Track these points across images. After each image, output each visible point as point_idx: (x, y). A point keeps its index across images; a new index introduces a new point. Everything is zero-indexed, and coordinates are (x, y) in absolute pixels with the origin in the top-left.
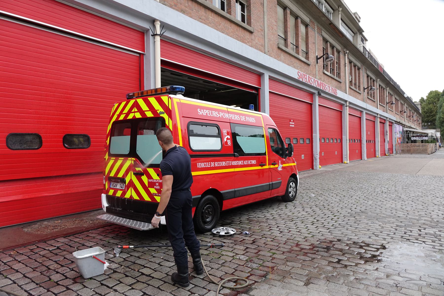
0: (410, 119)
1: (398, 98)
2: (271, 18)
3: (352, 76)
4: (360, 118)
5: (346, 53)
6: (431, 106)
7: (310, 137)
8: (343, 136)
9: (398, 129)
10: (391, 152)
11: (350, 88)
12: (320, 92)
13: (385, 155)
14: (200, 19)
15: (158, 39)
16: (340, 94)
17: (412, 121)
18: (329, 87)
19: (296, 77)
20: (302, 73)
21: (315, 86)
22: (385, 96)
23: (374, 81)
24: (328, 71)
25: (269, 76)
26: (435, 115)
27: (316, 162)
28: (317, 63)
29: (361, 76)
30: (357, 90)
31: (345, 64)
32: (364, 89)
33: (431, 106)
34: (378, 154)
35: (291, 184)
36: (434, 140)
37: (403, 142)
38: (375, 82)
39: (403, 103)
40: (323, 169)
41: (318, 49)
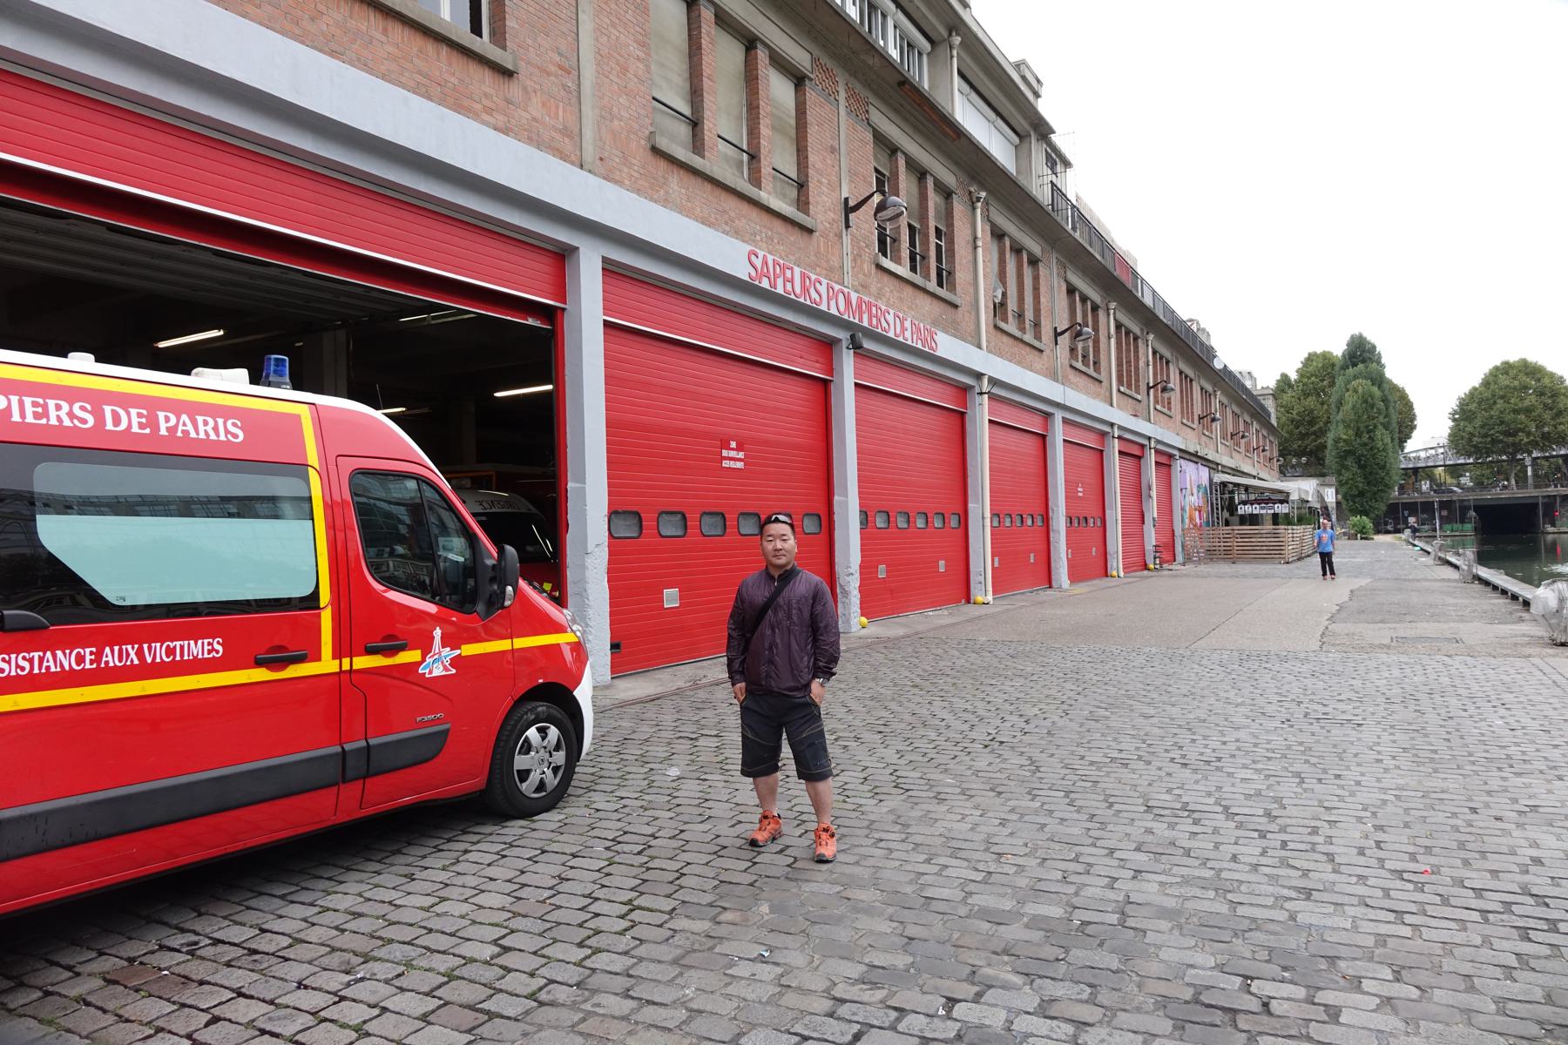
0: (1238, 445)
1: (1190, 373)
2: (614, 25)
3: (1004, 283)
4: (1044, 437)
5: (978, 199)
6: (1311, 402)
9: (1192, 480)
11: (996, 327)
12: (857, 337)
13: (1146, 567)
16: (949, 347)
17: (1242, 449)
18: (900, 319)
19: (742, 272)
20: (770, 258)
21: (834, 311)
22: (1141, 364)
23: (1095, 308)
24: (897, 260)
25: (605, 260)
26: (1322, 432)
27: (847, 606)
28: (848, 226)
29: (1043, 289)
30: (1028, 337)
31: (975, 238)
32: (1057, 334)
33: (1311, 402)
34: (1117, 564)
35: (532, 733)
36: (1309, 515)
37: (1211, 523)
38: (1101, 313)
39: (1209, 388)
40: (878, 629)
41: (853, 174)
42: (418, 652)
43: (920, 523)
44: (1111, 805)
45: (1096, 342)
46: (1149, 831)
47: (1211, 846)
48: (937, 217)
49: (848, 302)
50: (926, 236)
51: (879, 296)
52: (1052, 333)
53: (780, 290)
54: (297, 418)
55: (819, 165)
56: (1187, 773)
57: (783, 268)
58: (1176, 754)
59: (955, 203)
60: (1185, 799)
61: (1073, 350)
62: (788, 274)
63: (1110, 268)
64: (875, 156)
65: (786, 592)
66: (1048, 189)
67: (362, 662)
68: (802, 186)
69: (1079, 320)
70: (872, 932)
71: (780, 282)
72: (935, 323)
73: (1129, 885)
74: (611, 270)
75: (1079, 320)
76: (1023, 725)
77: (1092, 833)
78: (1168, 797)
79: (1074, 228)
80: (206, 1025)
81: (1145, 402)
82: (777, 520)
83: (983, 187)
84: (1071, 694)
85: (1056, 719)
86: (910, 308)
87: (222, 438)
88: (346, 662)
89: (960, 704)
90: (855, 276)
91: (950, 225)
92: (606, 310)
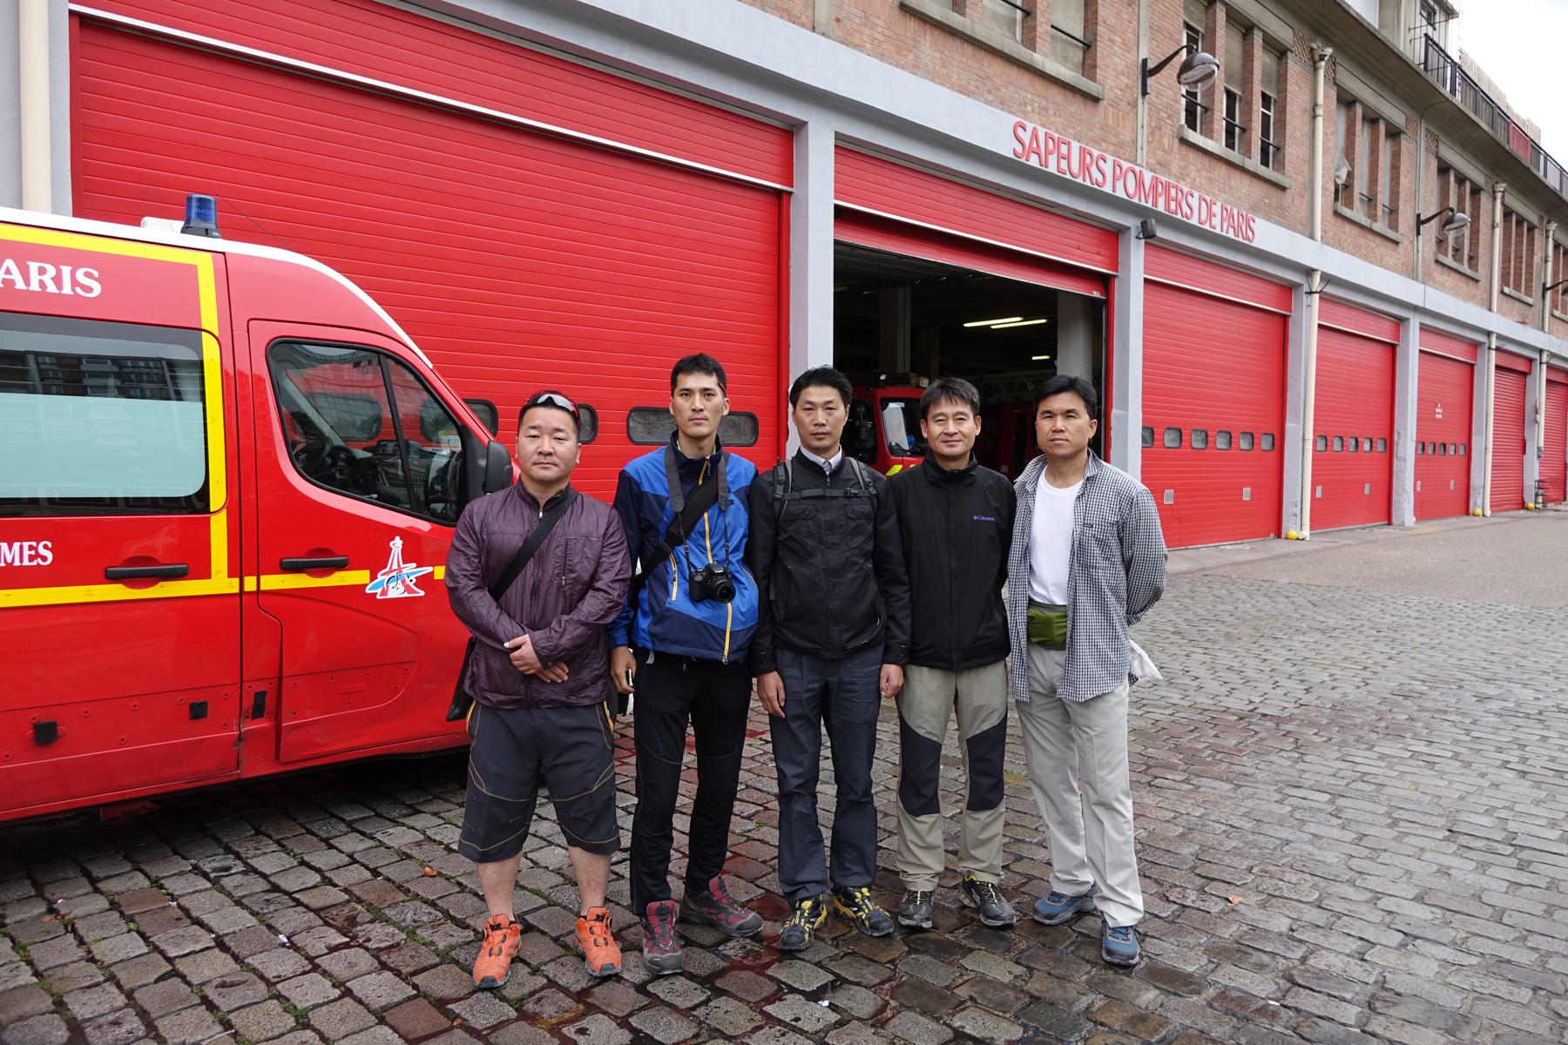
4: (1393, 347)
5: (1322, 58)
7: (1274, 429)
8: (1288, 425)
10: (1558, 495)
11: (1336, 213)
13: (1523, 506)
14: (1354, 251)
15: (1544, 367)
16: (1270, 236)
18: (1208, 202)
19: (1005, 147)
20: (1041, 132)
21: (1120, 193)
22: (1537, 259)
24: (1209, 134)
25: (838, 136)
28: (1145, 93)
29: (1404, 168)
30: (1379, 226)
31: (1315, 105)
32: (1420, 222)
34: (1482, 499)
38: (1485, 199)
42: (367, 573)
43: (1221, 443)
44: (1395, 823)
45: (1475, 232)
46: (1444, 871)
47: (1539, 909)
48: (1265, 82)
49: (1140, 183)
50: (1248, 104)
51: (1182, 176)
52: (1413, 222)
53: (1052, 169)
54: (192, 270)
55: (1111, 21)
56: (1524, 785)
57: (1058, 143)
58: (1513, 756)
59: (1290, 64)
60: (1512, 826)
61: (1441, 242)
62: (1064, 149)
63: (1503, 142)
64: (1186, 9)
65: (558, 528)
66: (1420, 45)
67: (272, 582)
68: (1088, 47)
69: (1453, 203)
70: (983, 979)
71: (1053, 159)
72: (1255, 209)
73: (1392, 959)
74: (845, 149)
75: (1453, 203)
76: (1301, 694)
77: (1353, 863)
78: (1485, 820)
79: (1453, 91)
80: (156, 981)
81: (1539, 306)
82: (550, 403)
83: (1328, 41)
84: (1380, 658)
85: (1349, 689)
86: (1222, 191)
87: (67, 290)
88: (250, 584)
89: (1225, 659)
90: (1151, 152)
91: (1282, 91)
92: (838, 193)
